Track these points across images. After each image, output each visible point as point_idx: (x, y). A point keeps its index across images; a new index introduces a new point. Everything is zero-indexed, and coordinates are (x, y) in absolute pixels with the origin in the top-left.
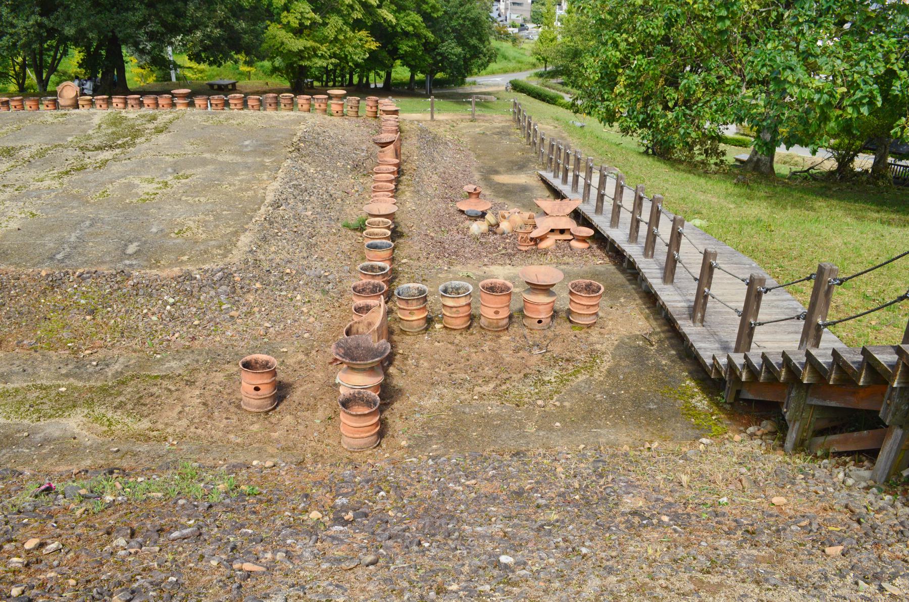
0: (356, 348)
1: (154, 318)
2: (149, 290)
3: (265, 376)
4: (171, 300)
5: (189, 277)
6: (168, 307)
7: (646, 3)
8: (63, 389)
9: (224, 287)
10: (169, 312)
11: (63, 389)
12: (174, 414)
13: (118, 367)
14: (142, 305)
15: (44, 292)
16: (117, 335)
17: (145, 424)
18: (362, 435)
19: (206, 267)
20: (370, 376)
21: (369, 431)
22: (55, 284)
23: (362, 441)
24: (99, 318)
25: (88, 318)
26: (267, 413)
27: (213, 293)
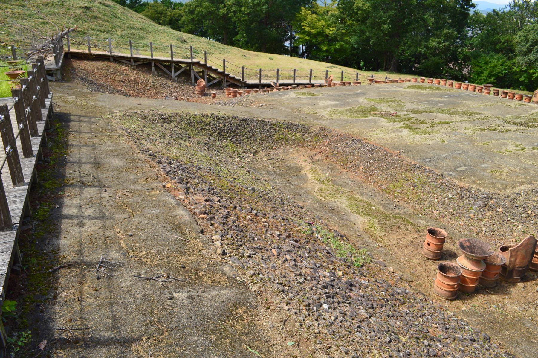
0: (479, 248)
1: (436, 200)
2: (445, 187)
3: (434, 239)
4: (450, 196)
5: (469, 190)
6: (446, 199)
7: (5, 58)
8: (374, 208)
9: (481, 202)
10: (445, 201)
11: (374, 208)
12: (396, 238)
13: (401, 211)
14: (437, 192)
15: (406, 171)
16: (415, 200)
17: (382, 235)
18: (441, 287)
19: (481, 189)
20: (473, 265)
21: (445, 287)
22: (414, 169)
23: (441, 291)
24: (415, 190)
25: (412, 188)
26: (428, 259)
27: (472, 202)
